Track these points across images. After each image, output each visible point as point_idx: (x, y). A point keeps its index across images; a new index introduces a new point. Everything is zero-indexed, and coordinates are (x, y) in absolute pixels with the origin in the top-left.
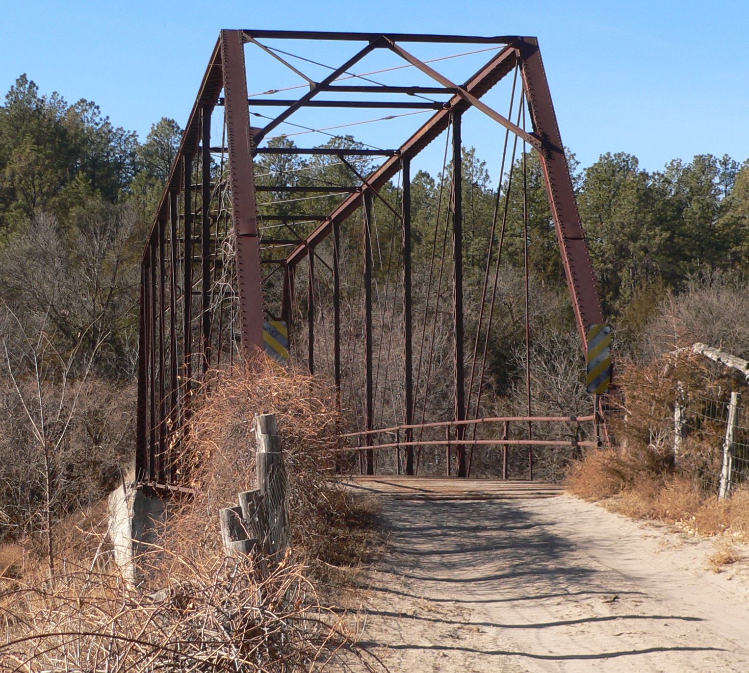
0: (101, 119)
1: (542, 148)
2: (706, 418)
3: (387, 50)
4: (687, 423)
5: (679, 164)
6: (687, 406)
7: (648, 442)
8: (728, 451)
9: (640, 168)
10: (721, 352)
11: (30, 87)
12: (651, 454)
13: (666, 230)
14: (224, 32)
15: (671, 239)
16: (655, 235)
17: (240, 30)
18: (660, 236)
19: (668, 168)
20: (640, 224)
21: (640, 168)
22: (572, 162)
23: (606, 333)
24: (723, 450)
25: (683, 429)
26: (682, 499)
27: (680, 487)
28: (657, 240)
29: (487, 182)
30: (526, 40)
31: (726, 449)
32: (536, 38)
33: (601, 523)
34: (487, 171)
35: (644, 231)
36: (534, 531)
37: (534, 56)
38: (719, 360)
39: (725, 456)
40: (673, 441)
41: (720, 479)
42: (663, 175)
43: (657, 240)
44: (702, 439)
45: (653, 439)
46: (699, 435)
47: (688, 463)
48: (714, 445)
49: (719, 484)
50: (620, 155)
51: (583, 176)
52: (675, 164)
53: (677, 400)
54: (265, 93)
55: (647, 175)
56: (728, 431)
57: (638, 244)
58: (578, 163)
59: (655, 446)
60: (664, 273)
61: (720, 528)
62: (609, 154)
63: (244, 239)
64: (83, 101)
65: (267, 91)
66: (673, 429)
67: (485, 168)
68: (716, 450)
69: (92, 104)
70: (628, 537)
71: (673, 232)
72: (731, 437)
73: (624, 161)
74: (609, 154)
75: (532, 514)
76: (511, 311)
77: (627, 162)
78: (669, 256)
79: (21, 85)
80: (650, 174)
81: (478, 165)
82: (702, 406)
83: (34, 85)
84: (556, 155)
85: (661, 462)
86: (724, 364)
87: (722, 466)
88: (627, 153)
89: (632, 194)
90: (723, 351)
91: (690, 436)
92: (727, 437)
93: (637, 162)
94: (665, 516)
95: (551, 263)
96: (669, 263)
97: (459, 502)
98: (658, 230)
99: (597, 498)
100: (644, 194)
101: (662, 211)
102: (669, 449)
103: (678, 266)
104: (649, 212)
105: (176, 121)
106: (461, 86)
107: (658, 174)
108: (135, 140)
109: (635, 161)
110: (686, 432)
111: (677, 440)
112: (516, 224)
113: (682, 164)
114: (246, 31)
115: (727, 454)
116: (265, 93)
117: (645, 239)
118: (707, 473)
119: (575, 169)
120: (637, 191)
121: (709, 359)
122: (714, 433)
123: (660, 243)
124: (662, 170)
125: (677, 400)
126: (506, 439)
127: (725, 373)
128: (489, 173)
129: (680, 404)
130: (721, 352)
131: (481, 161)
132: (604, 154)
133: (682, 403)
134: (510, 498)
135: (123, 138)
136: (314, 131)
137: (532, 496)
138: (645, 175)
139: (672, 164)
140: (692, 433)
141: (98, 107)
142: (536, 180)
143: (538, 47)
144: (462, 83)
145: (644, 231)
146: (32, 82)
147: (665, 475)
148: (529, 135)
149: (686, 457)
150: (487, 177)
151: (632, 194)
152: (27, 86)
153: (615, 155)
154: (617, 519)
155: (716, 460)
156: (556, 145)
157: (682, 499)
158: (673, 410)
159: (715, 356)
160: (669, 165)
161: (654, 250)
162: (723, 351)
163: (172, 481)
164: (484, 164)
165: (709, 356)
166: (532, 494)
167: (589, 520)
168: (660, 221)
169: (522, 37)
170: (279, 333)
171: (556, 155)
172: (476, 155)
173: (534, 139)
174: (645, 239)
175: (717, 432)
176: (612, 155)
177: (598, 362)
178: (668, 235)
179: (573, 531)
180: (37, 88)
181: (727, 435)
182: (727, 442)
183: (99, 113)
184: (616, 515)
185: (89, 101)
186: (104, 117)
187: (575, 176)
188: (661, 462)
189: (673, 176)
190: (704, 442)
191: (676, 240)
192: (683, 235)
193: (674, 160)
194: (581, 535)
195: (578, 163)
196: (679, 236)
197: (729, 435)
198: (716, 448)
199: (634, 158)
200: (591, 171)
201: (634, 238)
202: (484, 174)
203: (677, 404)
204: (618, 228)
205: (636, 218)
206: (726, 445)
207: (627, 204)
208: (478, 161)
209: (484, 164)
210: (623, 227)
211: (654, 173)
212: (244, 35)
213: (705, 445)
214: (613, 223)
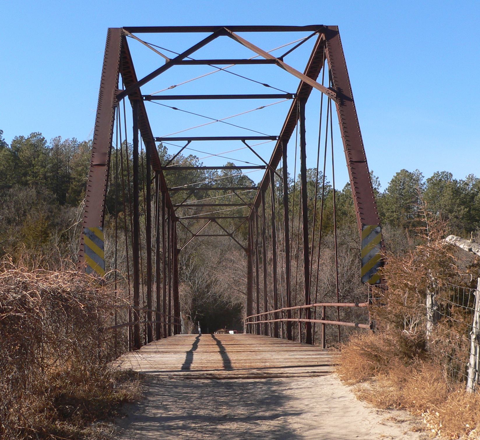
0: (199, 164)
1: (336, 98)
2: (453, 304)
3: (226, 38)
4: (438, 309)
5: (472, 176)
6: (437, 293)
7: (403, 328)
8: (475, 339)
9: (454, 178)
10: (472, 242)
11: (164, 149)
12: (404, 340)
13: (466, 208)
14: (110, 30)
15: (469, 212)
16: (461, 210)
17: (121, 28)
18: (464, 210)
19: (467, 178)
20: (453, 204)
21: (454, 178)
22: (421, 176)
23: (377, 232)
24: (470, 339)
25: (434, 316)
26: (429, 388)
27: (428, 375)
28: (462, 212)
29: (379, 187)
30: (329, 28)
31: (473, 337)
32: (337, 26)
33: (347, 414)
34: (379, 181)
35: (456, 208)
36: (277, 422)
37: (335, 38)
38: (470, 250)
39: (473, 344)
40: (426, 326)
41: (467, 368)
42: (464, 181)
43: (462, 212)
44: (451, 326)
45: (407, 325)
46: (448, 321)
47: (438, 349)
48: (462, 332)
49: (467, 374)
50: (443, 173)
51: (426, 183)
52: (470, 176)
53: (429, 287)
54: (169, 88)
55: (457, 181)
56: (475, 318)
57: (453, 214)
58: (423, 177)
59: (409, 332)
60: (466, 229)
61: (464, 429)
62: (438, 172)
63: (96, 167)
64: (191, 155)
65: (170, 87)
66: (425, 315)
67: (378, 180)
68: (464, 338)
69: (195, 156)
70: (367, 434)
71: (470, 209)
72: (478, 325)
73: (446, 175)
74: (438, 172)
75: (289, 398)
76: (390, 248)
77: (447, 175)
78: (468, 220)
79: (160, 148)
80: (458, 181)
81: (375, 179)
82: (451, 293)
83: (166, 148)
84: (347, 102)
85: (414, 347)
86: (475, 254)
87: (469, 355)
88: (447, 171)
89: (449, 190)
90: (473, 241)
91: (440, 322)
92: (474, 325)
93: (452, 175)
94: (413, 406)
95: (411, 224)
96: (468, 223)
97: (241, 381)
98: (462, 207)
99: (354, 381)
100: (455, 190)
101: (465, 198)
102: (422, 334)
103: (473, 224)
104: (458, 199)
105: (234, 163)
106: (278, 58)
107: (462, 181)
108: (217, 173)
109: (451, 175)
110: (436, 318)
111: (429, 326)
112: (393, 206)
113: (474, 176)
114: (125, 28)
115: (474, 342)
116: (169, 88)
117: (456, 212)
118: (455, 360)
119: (422, 180)
120: (452, 189)
121: (462, 250)
122: (462, 320)
123: (464, 214)
124: (464, 179)
125: (429, 287)
126: (323, 319)
127: (476, 262)
128: (380, 183)
129: (431, 292)
130: (472, 242)
131: (376, 177)
132: (436, 172)
133: (432, 290)
134: (287, 377)
135: (212, 173)
136: (217, 121)
137: (307, 375)
138: (456, 182)
139: (469, 176)
140: (442, 319)
141: (198, 158)
142: (403, 185)
143: (339, 32)
144: (280, 56)
145: (456, 208)
146: (165, 147)
147: (417, 360)
148: (327, 89)
149: (437, 342)
150: (379, 184)
151: (449, 190)
152: (163, 148)
153: (441, 173)
154: (363, 409)
155: (464, 348)
156: (348, 96)
157: (429, 388)
158: (425, 296)
159: (466, 247)
160: (468, 177)
161: (461, 217)
162: (473, 241)
163: (350, 312)
164: (378, 178)
165: (462, 246)
166: (308, 372)
167: (337, 410)
168: (463, 203)
169: (327, 26)
170: (97, 237)
171: (347, 102)
172: (374, 174)
173: (330, 91)
174: (456, 212)
175: (465, 318)
176: (440, 172)
177: (370, 257)
178: (467, 210)
179: (315, 423)
180: (167, 149)
181: (474, 322)
182: (474, 330)
183: (199, 161)
184: (364, 403)
185: (194, 155)
186: (201, 163)
187: (422, 183)
188: (414, 347)
189: (470, 182)
190: (453, 328)
191: (471, 212)
192: (475, 209)
193: (470, 175)
194: (319, 431)
195: (423, 177)
196: (473, 210)
197: (476, 323)
198: (464, 336)
199: (450, 173)
200: (429, 180)
201: (451, 211)
202: (378, 183)
203: (429, 292)
204: (443, 207)
205: (452, 202)
206: (473, 333)
207: (448, 194)
208: (375, 177)
209: (378, 178)
210: (445, 206)
211: (460, 180)
212: (124, 30)
213: (453, 331)
214: (440, 205)
